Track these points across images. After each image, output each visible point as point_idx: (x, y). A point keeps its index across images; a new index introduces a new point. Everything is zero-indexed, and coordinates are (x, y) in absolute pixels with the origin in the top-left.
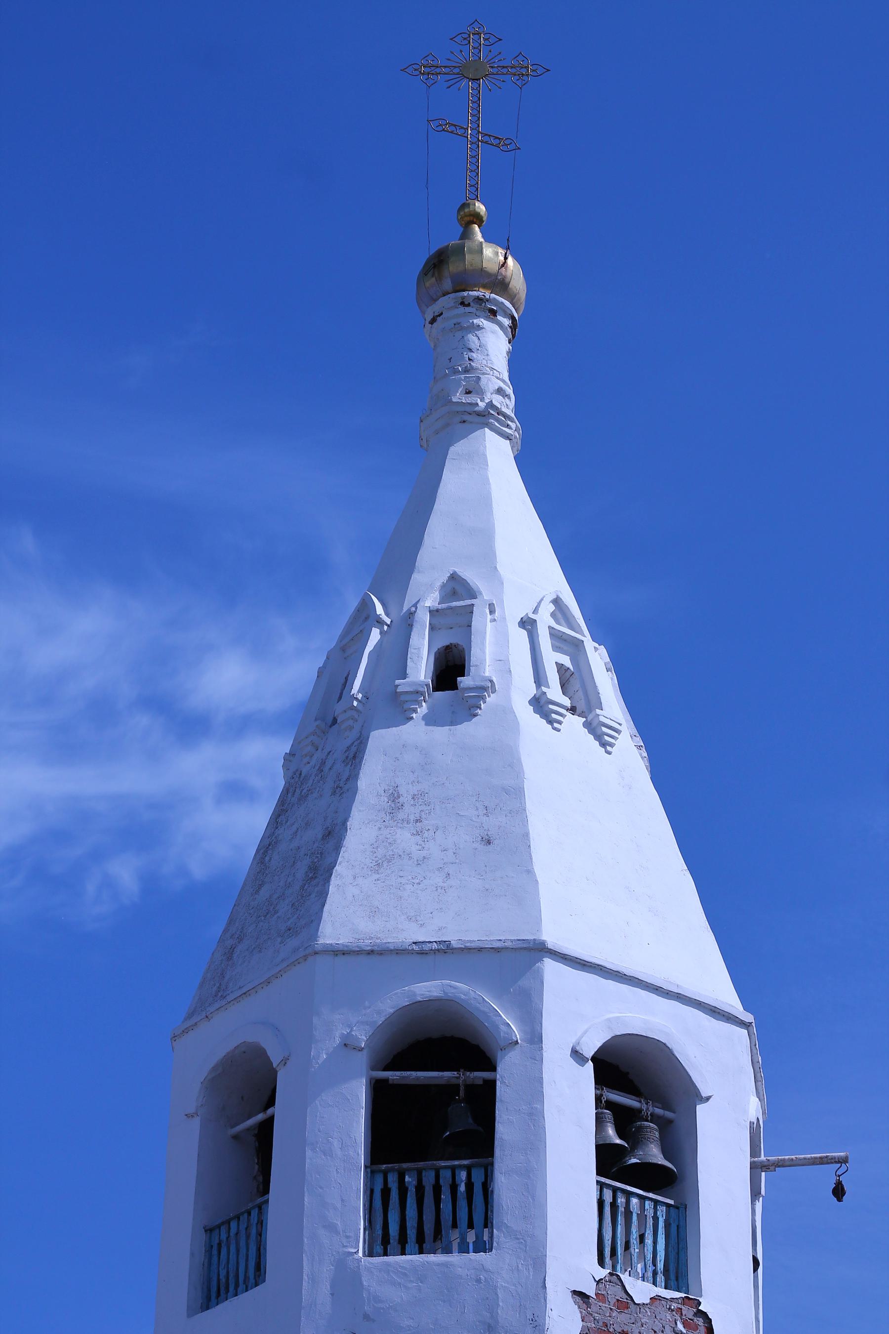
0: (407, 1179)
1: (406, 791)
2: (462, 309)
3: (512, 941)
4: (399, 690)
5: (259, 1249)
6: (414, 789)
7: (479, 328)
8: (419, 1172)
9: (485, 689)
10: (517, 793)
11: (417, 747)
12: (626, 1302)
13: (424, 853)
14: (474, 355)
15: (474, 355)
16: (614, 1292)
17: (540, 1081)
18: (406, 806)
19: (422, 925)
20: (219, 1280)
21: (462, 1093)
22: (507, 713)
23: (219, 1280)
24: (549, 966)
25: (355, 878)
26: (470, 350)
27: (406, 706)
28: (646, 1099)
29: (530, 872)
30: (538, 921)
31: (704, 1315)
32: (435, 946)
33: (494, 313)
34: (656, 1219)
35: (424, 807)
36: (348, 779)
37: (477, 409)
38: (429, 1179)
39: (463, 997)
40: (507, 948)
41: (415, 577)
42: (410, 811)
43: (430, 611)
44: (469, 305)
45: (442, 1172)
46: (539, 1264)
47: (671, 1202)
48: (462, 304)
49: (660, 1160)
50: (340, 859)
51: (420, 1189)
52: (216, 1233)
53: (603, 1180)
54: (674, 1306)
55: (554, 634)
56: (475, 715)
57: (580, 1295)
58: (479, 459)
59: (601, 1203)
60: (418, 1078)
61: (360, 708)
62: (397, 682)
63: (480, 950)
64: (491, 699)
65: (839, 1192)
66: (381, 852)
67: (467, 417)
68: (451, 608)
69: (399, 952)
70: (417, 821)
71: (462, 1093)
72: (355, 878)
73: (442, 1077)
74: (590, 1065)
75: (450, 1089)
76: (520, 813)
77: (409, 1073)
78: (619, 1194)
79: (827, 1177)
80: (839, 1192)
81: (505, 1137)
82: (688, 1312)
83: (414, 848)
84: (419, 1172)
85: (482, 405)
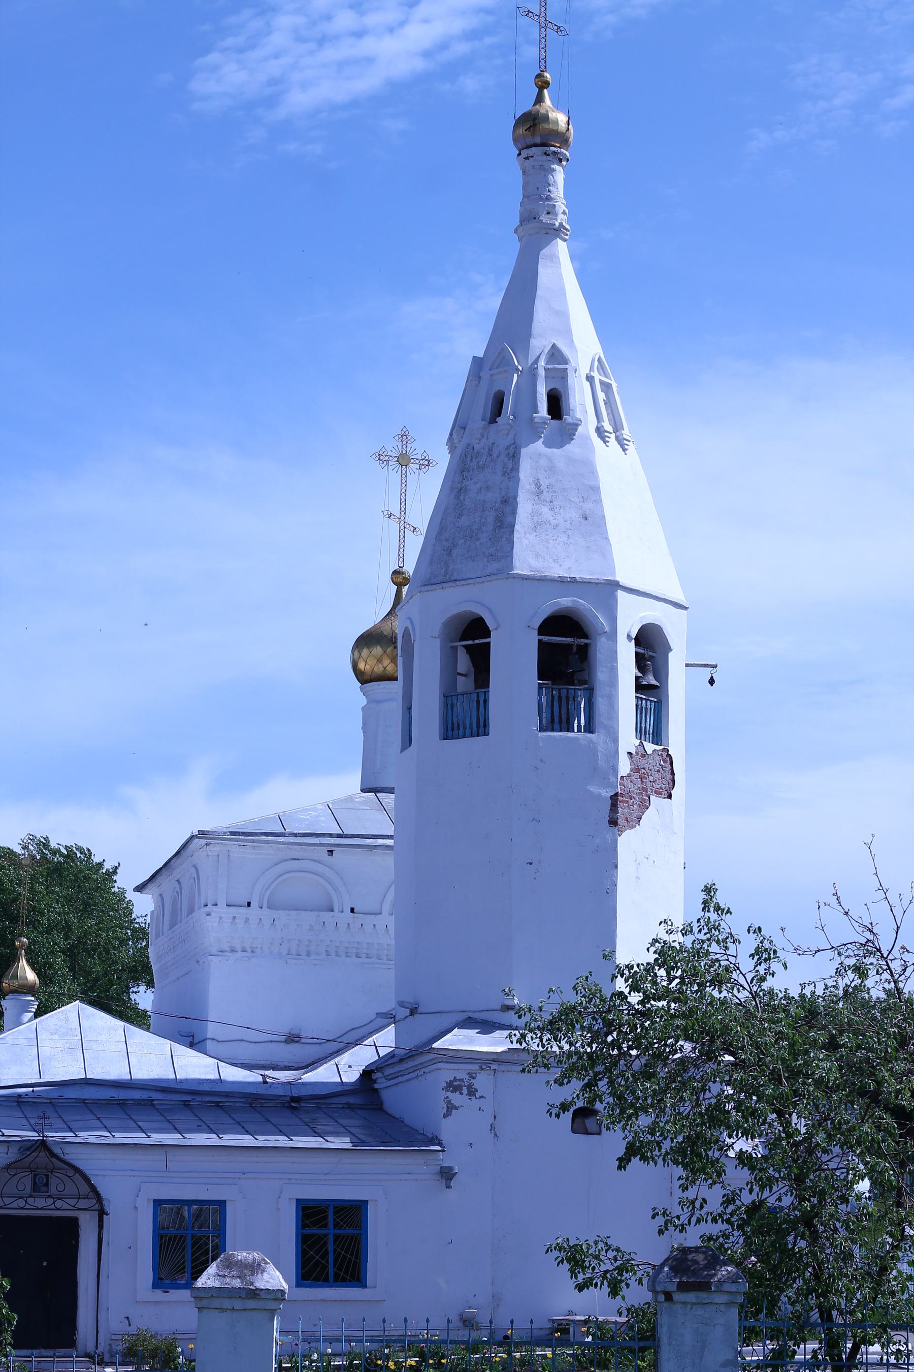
0: (554, 692)
1: (544, 483)
2: (545, 157)
3: (604, 580)
4: (536, 420)
5: (485, 721)
6: (547, 482)
7: (554, 170)
8: (560, 689)
9: (576, 426)
10: (596, 490)
11: (546, 456)
12: (645, 755)
13: (556, 522)
14: (551, 188)
15: (551, 188)
16: (641, 751)
17: (616, 651)
18: (544, 492)
19: (561, 565)
20: (453, 723)
21: (575, 649)
22: (588, 438)
23: (453, 723)
24: (620, 594)
25: (525, 534)
26: (549, 185)
27: (539, 430)
28: (647, 648)
29: (607, 538)
30: (613, 569)
31: (669, 756)
32: (569, 579)
33: (561, 160)
34: (651, 708)
35: (552, 494)
36: (512, 470)
37: (554, 227)
38: (564, 693)
39: (582, 607)
40: (601, 583)
41: (532, 340)
42: (546, 495)
43: (545, 369)
44: (549, 155)
45: (570, 690)
46: (616, 741)
47: (656, 700)
48: (545, 153)
49: (654, 682)
50: (517, 522)
51: (560, 698)
52: (449, 699)
53: (639, 695)
54: (660, 753)
55: (602, 383)
56: (573, 439)
57: (630, 754)
58: (554, 258)
59: (637, 706)
60: (556, 640)
61: (512, 424)
62: (534, 415)
63: (589, 583)
64: (580, 429)
65: (712, 681)
66: (535, 519)
67: (549, 231)
68: (555, 369)
69: (552, 580)
70: (551, 502)
71: (575, 649)
72: (525, 534)
73: (567, 641)
74: (633, 641)
75: (570, 646)
76: (599, 502)
77: (552, 638)
78: (639, 700)
79: (706, 673)
80: (712, 681)
81: (601, 678)
82: (665, 754)
83: (551, 518)
84: (560, 689)
85: (557, 224)
